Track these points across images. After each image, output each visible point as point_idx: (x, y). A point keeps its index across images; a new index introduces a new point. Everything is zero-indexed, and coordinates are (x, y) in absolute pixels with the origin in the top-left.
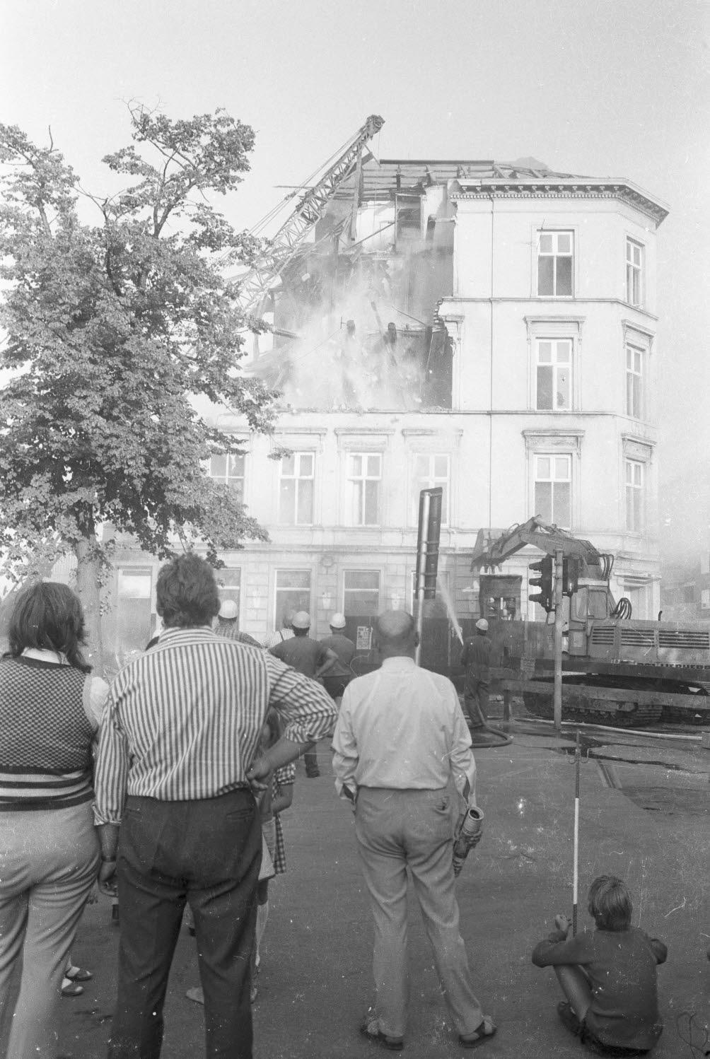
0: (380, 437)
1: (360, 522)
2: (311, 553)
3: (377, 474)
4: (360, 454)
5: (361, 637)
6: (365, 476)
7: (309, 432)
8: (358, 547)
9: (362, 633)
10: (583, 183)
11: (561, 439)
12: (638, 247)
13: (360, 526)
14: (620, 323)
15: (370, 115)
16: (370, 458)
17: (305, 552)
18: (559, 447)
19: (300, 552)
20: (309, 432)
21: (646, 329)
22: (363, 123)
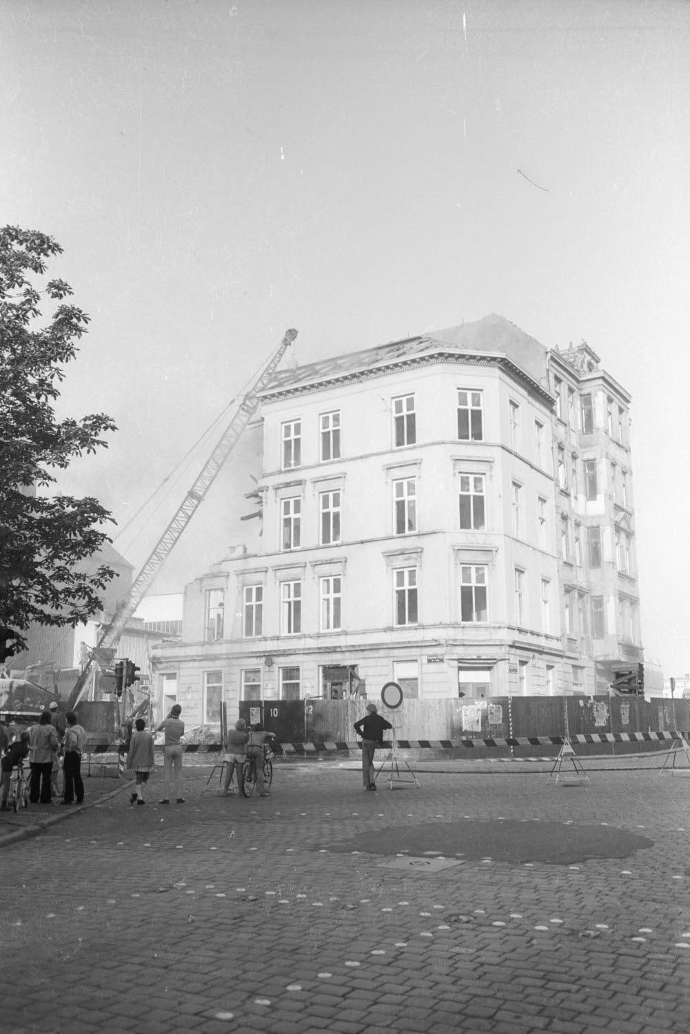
0: (297, 569)
1: (289, 631)
2: (260, 657)
3: (414, 584)
4: (328, 578)
5: (253, 715)
6: (293, 599)
7: (257, 571)
8: (284, 651)
9: (254, 712)
10: (422, 356)
11: (407, 556)
12: (593, 362)
13: (289, 635)
14: (450, 459)
15: (287, 330)
16: (334, 580)
17: (257, 657)
18: (406, 562)
19: (252, 657)
20: (257, 571)
21: (479, 457)
22: (283, 335)
